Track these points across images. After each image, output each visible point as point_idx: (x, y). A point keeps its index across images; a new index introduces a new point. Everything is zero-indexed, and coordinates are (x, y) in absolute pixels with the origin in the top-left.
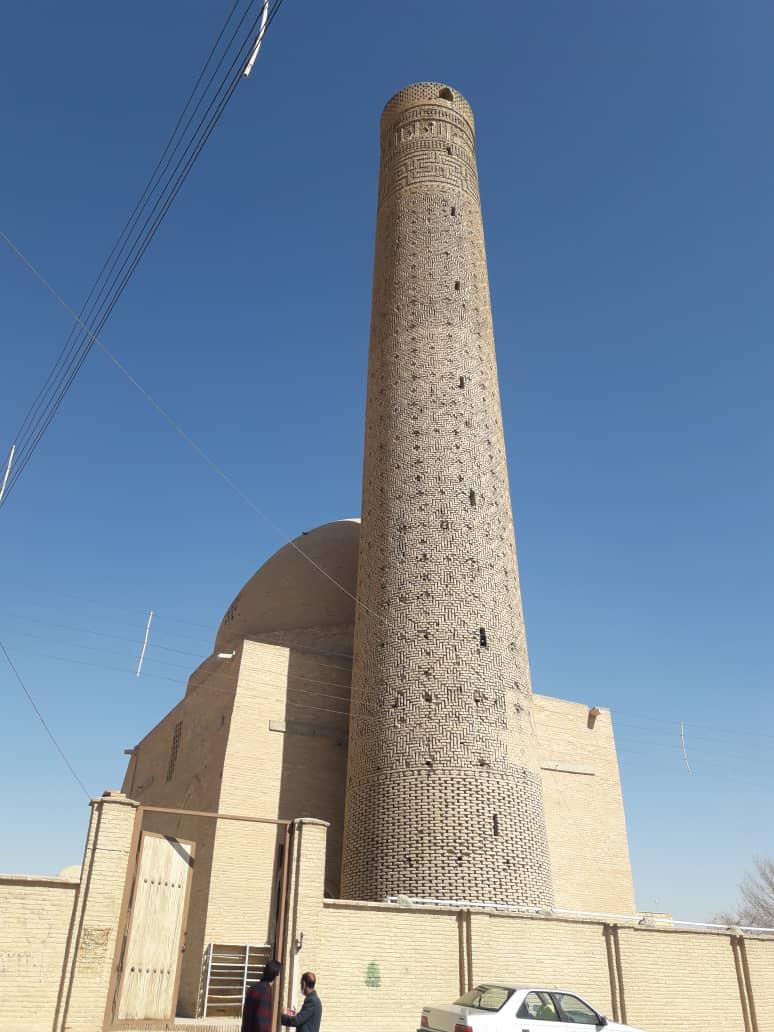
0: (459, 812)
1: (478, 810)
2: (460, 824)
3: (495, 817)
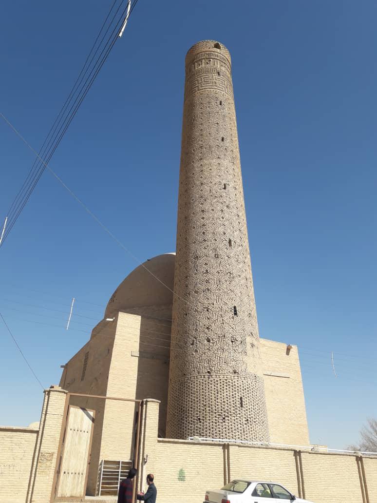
0: (223, 396)
1: (233, 395)
2: (224, 402)
3: (241, 398)
